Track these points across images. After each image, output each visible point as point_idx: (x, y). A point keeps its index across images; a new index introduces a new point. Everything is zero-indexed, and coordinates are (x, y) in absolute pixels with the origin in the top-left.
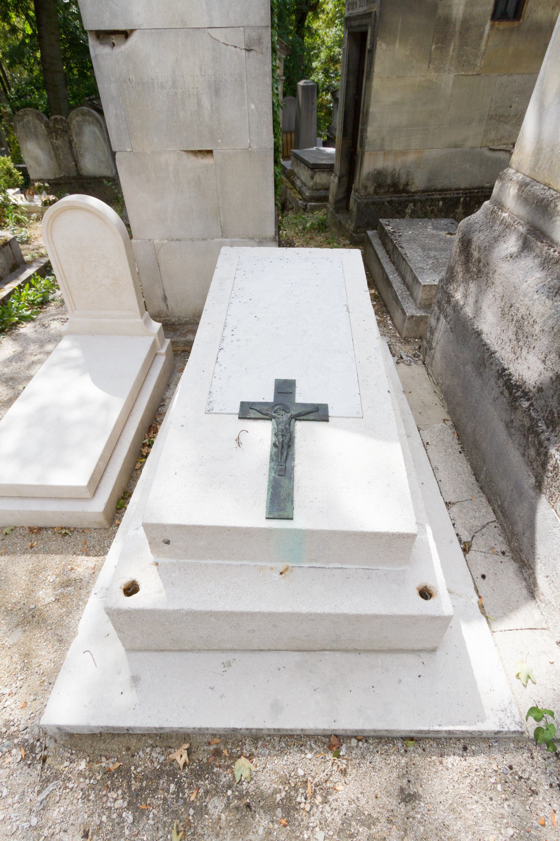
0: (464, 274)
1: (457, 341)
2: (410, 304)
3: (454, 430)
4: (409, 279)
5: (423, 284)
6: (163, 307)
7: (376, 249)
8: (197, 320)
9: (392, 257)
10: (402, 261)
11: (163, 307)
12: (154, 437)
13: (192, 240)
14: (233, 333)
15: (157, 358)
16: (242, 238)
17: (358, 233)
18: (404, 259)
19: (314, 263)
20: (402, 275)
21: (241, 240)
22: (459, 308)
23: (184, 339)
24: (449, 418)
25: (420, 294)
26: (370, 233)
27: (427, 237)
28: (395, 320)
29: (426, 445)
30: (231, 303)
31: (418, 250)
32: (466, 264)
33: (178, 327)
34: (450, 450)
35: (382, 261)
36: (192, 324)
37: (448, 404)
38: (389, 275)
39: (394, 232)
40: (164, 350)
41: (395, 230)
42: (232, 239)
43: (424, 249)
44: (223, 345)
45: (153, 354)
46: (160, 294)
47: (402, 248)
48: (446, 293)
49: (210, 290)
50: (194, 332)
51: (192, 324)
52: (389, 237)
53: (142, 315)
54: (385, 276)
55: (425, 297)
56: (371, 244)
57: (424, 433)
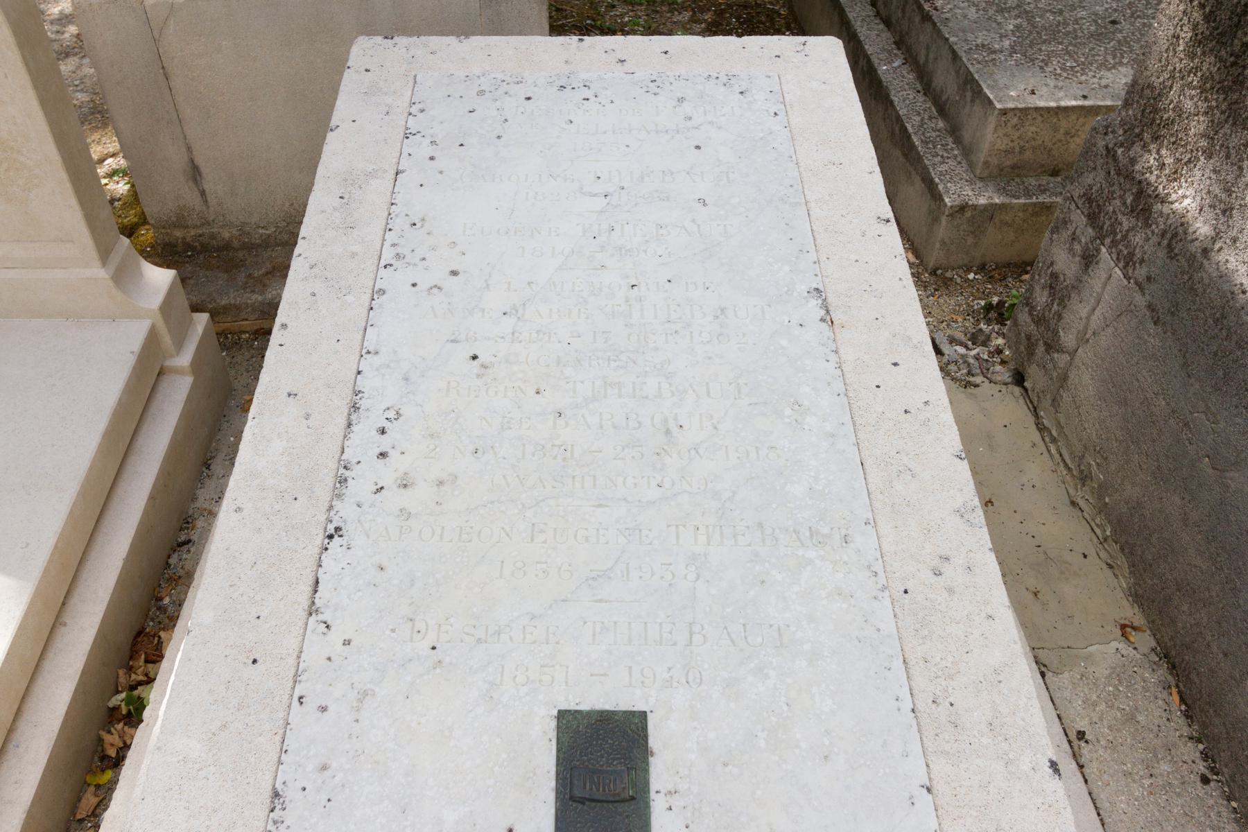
0: (1215, 126)
1: (1185, 365)
2: (952, 163)
3: (1163, 672)
4: (945, 79)
5: (999, 106)
10: (917, 19)
11: (197, 201)
12: (150, 680)
14: (385, 443)
15: (166, 380)
18: (926, 18)
19: (681, 100)
22: (1195, 248)
23: (257, 298)
24: (1139, 620)
25: (989, 138)
29: (1076, 742)
30: (382, 292)
32: (1225, 91)
33: (240, 254)
34: (1165, 767)
35: (851, 16)
37: (1132, 565)
38: (875, 61)
40: (185, 359)
44: (345, 511)
45: (149, 373)
48: (1129, 176)
49: (303, 232)
53: (104, 254)
54: (862, 62)
55: (1002, 145)
57: (1063, 681)
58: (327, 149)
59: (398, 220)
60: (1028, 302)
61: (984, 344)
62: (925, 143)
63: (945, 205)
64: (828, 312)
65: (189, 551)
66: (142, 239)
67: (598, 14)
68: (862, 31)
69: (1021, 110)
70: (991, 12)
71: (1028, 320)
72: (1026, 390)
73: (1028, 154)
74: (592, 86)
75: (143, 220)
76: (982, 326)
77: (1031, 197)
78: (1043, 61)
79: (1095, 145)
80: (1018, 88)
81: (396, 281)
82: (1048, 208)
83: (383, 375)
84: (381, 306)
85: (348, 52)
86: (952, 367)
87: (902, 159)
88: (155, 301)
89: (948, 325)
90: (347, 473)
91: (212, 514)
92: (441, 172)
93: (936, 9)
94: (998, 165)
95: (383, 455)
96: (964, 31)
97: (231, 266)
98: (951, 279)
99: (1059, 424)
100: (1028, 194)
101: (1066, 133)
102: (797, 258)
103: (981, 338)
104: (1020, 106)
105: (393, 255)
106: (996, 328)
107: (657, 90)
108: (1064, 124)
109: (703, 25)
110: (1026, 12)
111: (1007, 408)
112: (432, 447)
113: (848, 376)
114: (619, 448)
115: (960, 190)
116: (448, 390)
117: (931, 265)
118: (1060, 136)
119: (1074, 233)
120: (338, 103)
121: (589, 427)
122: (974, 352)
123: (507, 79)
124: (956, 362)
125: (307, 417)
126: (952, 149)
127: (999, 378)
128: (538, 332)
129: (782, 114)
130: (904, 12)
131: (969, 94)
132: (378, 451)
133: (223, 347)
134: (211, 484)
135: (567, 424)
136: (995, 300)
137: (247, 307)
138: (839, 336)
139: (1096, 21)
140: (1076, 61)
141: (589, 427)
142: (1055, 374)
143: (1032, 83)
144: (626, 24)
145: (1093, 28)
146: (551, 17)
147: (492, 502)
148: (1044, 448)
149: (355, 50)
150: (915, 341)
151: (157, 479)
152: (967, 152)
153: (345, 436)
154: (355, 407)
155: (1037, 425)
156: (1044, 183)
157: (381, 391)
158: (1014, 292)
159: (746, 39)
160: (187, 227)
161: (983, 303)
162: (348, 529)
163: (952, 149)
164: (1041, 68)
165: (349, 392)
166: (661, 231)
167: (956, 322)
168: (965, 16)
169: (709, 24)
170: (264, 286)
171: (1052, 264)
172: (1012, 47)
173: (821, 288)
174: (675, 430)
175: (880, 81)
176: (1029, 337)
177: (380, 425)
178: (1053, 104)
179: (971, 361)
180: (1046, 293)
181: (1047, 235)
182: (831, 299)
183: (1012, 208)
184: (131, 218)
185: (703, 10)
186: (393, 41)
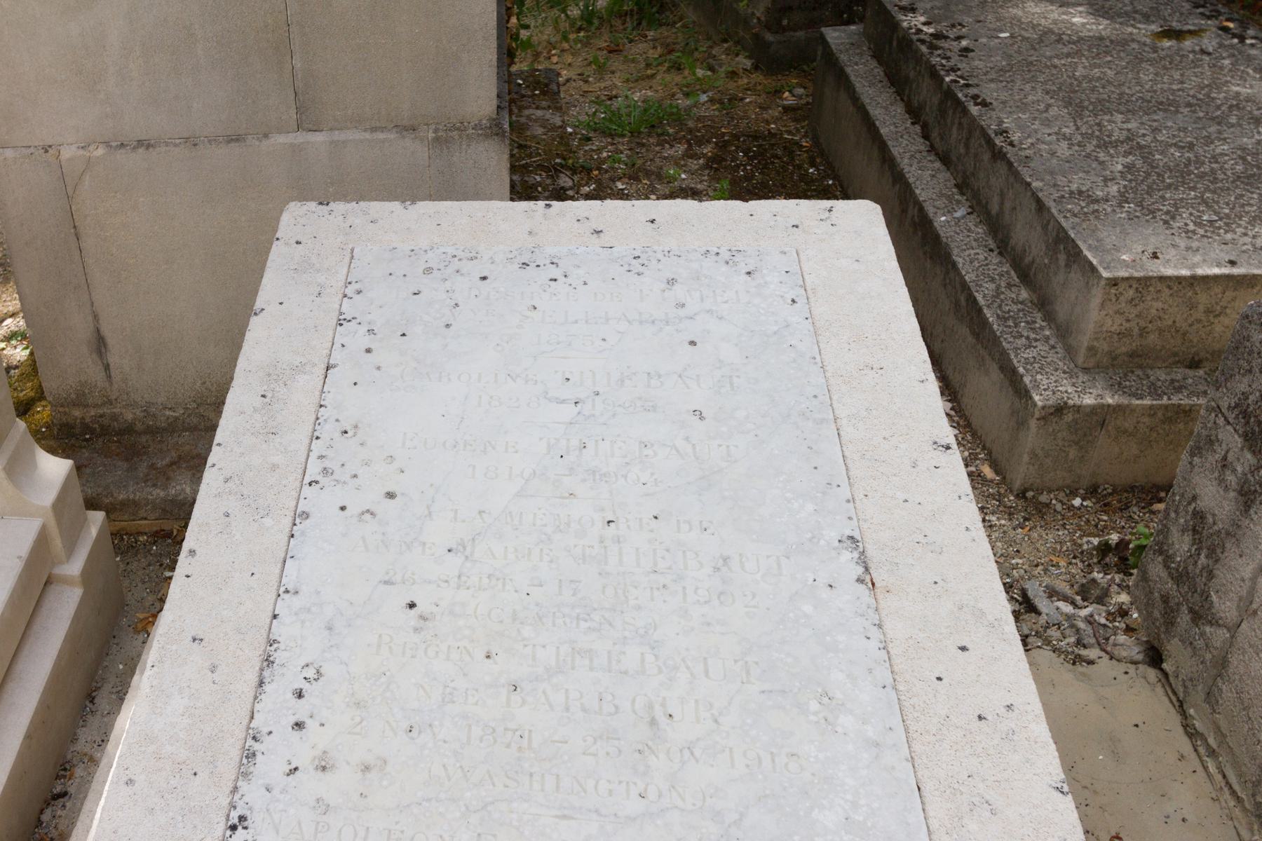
4: (1026, 234)
5: (1105, 274)
6: (95, 374)
7: (866, 100)
8: (212, 416)
9: (934, 135)
10: (986, 157)
11: (97, 375)
13: (191, 142)
14: (301, 710)
16: (374, 130)
17: (784, 30)
18: (998, 155)
19: (671, 282)
20: (988, 213)
21: (367, 135)
23: (159, 493)
25: (1094, 317)
26: (835, 36)
27: (1078, 53)
28: (966, 401)
30: (305, 515)
31: (1054, 111)
33: (143, 439)
35: (895, 151)
36: (193, 429)
38: (930, 210)
39: (938, 36)
40: (75, 567)
41: (943, 27)
42: (337, 136)
43: (1078, 110)
44: (252, 793)
45: (37, 579)
46: (81, 327)
47: (985, 104)
50: (196, 463)
51: (193, 429)
52: (918, 58)
54: (913, 212)
55: (1113, 324)
56: (842, 78)
58: (249, 336)
59: (327, 427)
60: (1162, 549)
61: (1101, 600)
62: (1003, 319)
63: (1035, 405)
64: (867, 569)
65: (64, 806)
66: (37, 417)
67: (571, 151)
68: (912, 171)
69: (1139, 280)
70: (1089, 148)
71: (1164, 574)
72: (1166, 675)
73: (1152, 338)
74: (561, 263)
75: (40, 395)
76: (1097, 575)
77: (1160, 397)
78: (1168, 213)
79: (1248, 339)
80: (1137, 250)
81: (320, 502)
82: (1187, 413)
83: (303, 622)
84: (303, 533)
85: (278, 220)
86: (1053, 633)
87: (971, 339)
88: (47, 497)
89: (1046, 570)
90: (256, 746)
91: (93, 761)
92: (379, 368)
93: (1012, 144)
94: (1110, 353)
95: (299, 725)
96: (1052, 173)
97: (132, 453)
98: (1048, 505)
99: (1218, 729)
100: (1155, 391)
101: (1208, 311)
102: (824, 493)
103: (1095, 592)
104: (1136, 275)
105: (319, 469)
106: (1118, 578)
107: (641, 269)
108: (1203, 299)
109: (701, 161)
110: (1140, 147)
111: (1135, 700)
112: (358, 719)
113: (896, 661)
114: (590, 740)
115: (1052, 385)
116: (379, 646)
117: (1017, 485)
118: (1199, 314)
119: (1225, 458)
120: (264, 281)
121: (551, 706)
122: (1084, 612)
123: (460, 254)
124: (1059, 625)
125: (213, 669)
126: (1042, 328)
127: (1124, 654)
128: (489, 577)
129: (801, 301)
130: (967, 147)
131: (1062, 258)
132: (293, 720)
133: (117, 550)
134: (94, 721)
135: (524, 702)
136: (1114, 538)
137: (146, 505)
138: (882, 603)
139: (1243, 159)
140: (1216, 213)
141: (551, 706)
142: (1208, 656)
143: (1153, 243)
144: (604, 161)
145: (1239, 168)
146: (512, 156)
147: (429, 800)
148: (1196, 763)
149: (285, 218)
150: (991, 618)
151: (36, 713)
152: (1064, 332)
153: (256, 698)
154: (268, 661)
155: (1185, 727)
156: (1179, 377)
157: (300, 641)
158: (1141, 528)
159: (754, 204)
160: (87, 406)
161: (1096, 541)
162: (255, 820)
163: (1042, 328)
164: (1166, 222)
165: (262, 639)
166: (646, 452)
167: (1057, 566)
168: (1053, 154)
169: (709, 159)
170: (168, 479)
171: (1194, 498)
172: (1122, 194)
173: (857, 536)
174: (663, 720)
175: (937, 237)
176: (1165, 599)
177: (297, 686)
178: (1185, 272)
179: (1082, 625)
180: (1187, 538)
181: (1185, 456)
182: (871, 552)
183: (1133, 411)
184: (27, 392)
185: (700, 142)
186: (328, 208)
